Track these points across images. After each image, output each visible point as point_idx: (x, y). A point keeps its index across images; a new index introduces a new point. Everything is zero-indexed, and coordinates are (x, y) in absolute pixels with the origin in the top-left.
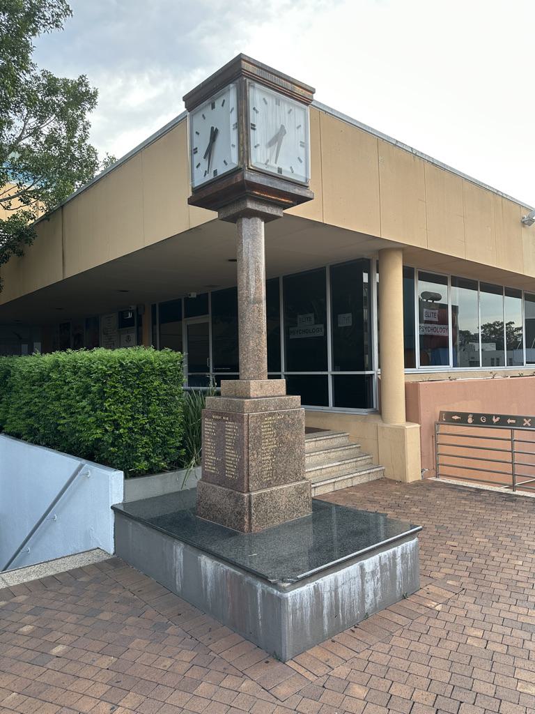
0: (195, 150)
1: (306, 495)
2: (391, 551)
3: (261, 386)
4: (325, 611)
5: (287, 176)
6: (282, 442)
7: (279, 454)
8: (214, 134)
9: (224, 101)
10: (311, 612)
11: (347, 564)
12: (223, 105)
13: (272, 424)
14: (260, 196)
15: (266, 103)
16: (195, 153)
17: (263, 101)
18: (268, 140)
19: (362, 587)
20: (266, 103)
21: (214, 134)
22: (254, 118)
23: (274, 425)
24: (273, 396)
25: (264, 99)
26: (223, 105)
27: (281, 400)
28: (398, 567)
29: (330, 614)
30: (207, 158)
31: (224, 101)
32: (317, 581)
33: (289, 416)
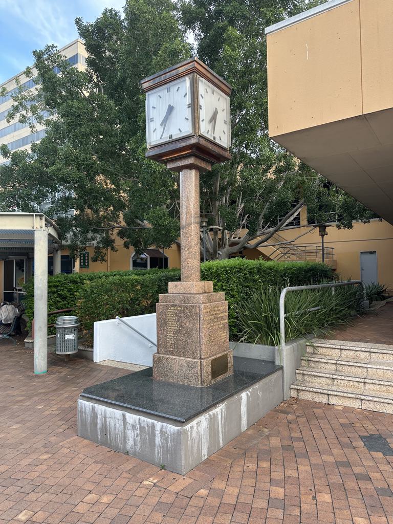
0: (151, 119)
1: (196, 371)
2: (150, 421)
3: (176, 286)
4: (99, 426)
5: (223, 145)
6: (181, 326)
7: (179, 334)
8: (171, 109)
9: (179, 88)
10: (91, 419)
11: (150, 417)
12: (177, 91)
13: (174, 313)
14: (167, 159)
15: (207, 92)
16: (151, 121)
17: (179, 91)
18: (210, 118)
19: (124, 432)
20: (207, 92)
21: (171, 109)
22: (202, 102)
23: (176, 314)
24: (179, 294)
25: (206, 90)
26: (177, 91)
27: (185, 297)
28: (157, 438)
29: (102, 429)
30: (213, 122)
31: (179, 88)
32: (95, 405)
33: (187, 309)
